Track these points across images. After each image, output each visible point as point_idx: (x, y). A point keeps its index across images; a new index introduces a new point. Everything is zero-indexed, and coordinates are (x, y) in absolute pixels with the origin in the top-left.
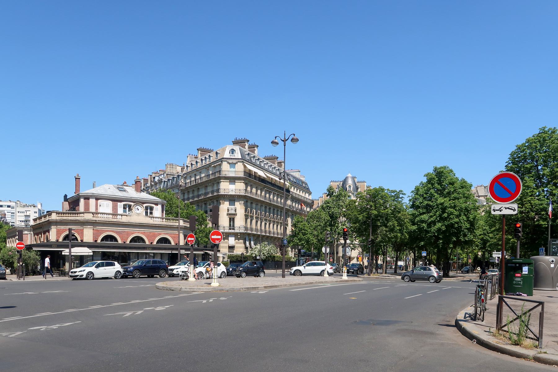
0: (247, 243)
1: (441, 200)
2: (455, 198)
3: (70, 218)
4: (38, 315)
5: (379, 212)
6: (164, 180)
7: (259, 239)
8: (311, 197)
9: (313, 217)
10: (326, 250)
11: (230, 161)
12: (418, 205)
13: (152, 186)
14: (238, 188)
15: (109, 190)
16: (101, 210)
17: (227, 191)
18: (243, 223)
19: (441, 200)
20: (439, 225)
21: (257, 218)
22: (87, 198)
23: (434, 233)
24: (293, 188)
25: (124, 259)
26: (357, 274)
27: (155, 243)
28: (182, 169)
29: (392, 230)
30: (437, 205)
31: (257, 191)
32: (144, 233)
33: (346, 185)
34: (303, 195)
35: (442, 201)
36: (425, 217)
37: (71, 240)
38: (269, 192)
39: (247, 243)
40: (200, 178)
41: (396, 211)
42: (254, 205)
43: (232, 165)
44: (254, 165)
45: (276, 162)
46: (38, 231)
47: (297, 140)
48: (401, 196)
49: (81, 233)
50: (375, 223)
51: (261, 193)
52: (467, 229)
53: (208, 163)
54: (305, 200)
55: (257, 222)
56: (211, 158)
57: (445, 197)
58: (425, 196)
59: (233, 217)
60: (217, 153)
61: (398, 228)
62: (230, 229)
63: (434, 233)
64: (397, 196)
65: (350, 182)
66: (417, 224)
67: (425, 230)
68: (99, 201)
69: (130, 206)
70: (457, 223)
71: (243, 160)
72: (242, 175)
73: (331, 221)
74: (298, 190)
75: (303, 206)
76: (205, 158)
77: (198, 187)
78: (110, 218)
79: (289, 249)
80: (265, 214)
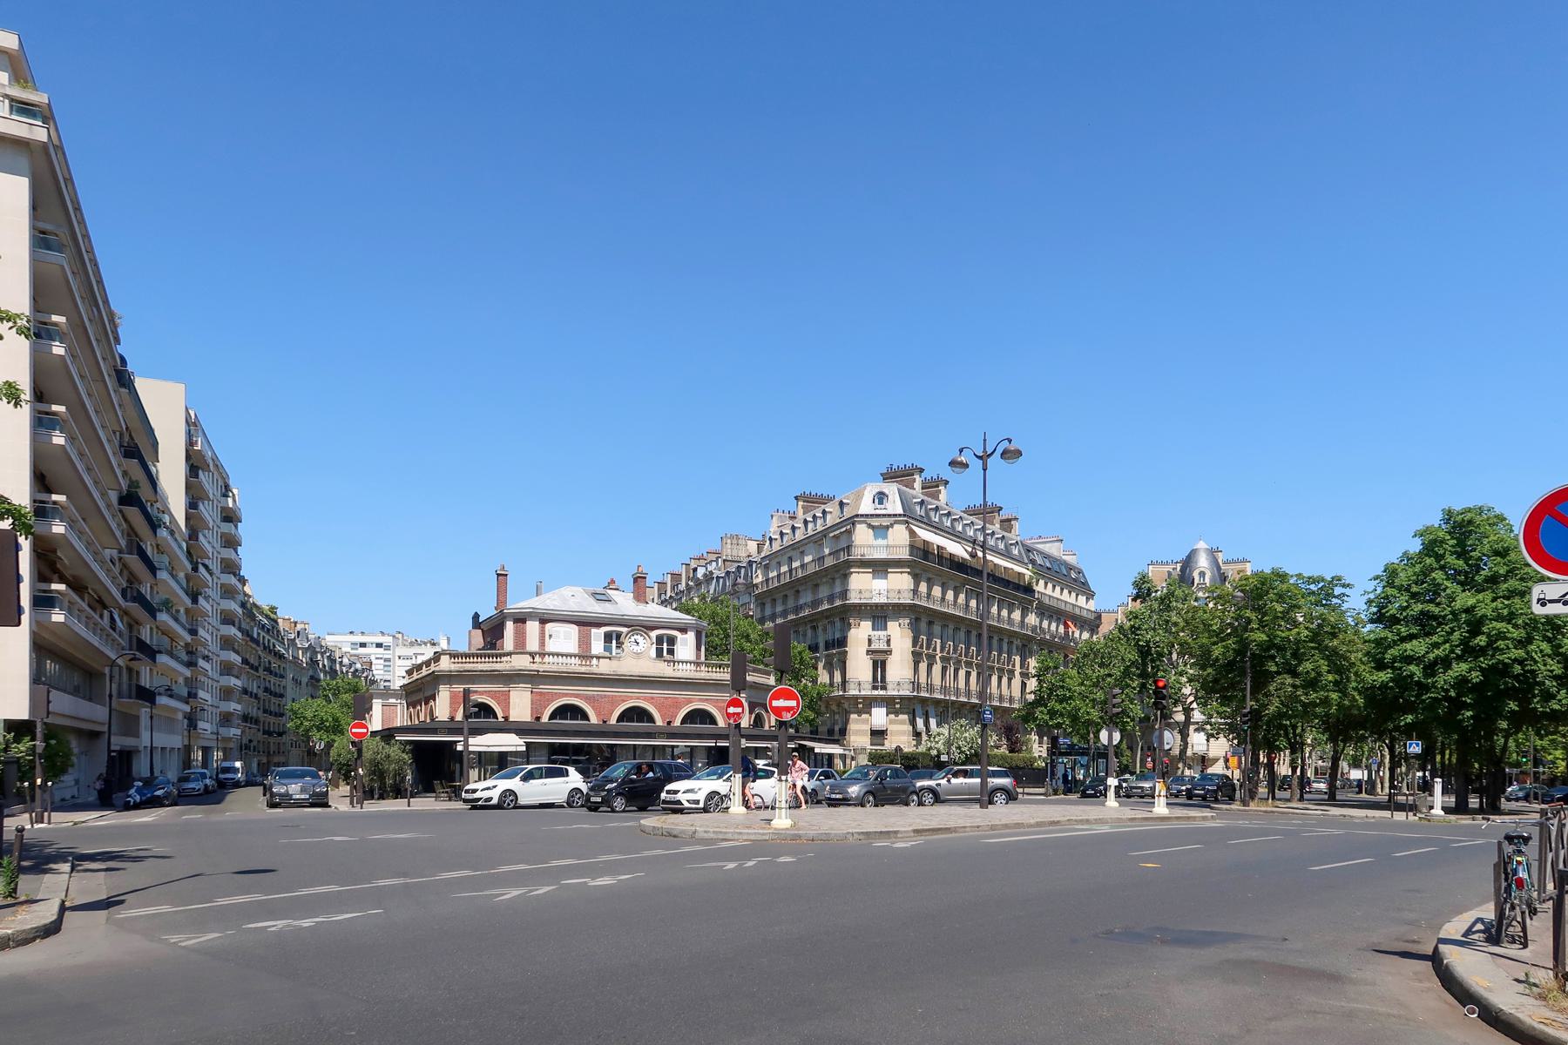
0: (920, 722)
1: (1465, 599)
2: (1511, 594)
3: (480, 667)
4: (305, 892)
5: (1272, 637)
6: (716, 573)
7: (947, 710)
8: (1092, 605)
9: (1091, 652)
10: (1110, 738)
11: (875, 522)
12: (1393, 616)
13: (689, 588)
14: (896, 587)
15: (573, 598)
16: (551, 646)
17: (867, 595)
18: (908, 673)
19: (1465, 599)
20: (1460, 668)
21: (944, 660)
22: (520, 620)
23: (1447, 691)
24: (1042, 582)
25: (589, 759)
26: (1216, 801)
27: (677, 723)
28: (760, 547)
29: (1312, 684)
30: (1452, 613)
31: (944, 594)
32: (651, 700)
33: (1191, 572)
34: (1072, 599)
35: (1471, 602)
36: (1417, 647)
37: (482, 716)
38: (974, 596)
39: (920, 722)
40: (803, 566)
41: (1324, 635)
42: (937, 629)
43: (881, 531)
44: (937, 528)
45: (997, 520)
46: (414, 698)
47: (1018, 453)
48: (1338, 591)
49: (505, 700)
50: (1263, 665)
51: (956, 597)
52: (1556, 678)
53: (820, 528)
54: (1077, 611)
55: (944, 669)
56: (828, 517)
57: (1479, 591)
58: (1415, 589)
59: (880, 657)
60: (841, 504)
61: (1330, 678)
62: (875, 688)
63: (1447, 691)
64: (1326, 591)
65: (1203, 562)
66: (1393, 668)
67: (1419, 683)
68: (549, 626)
69: (619, 636)
70: (1521, 662)
71: (907, 517)
72: (904, 554)
73: (1145, 664)
74: (1050, 586)
75: (1072, 628)
76: (814, 517)
77: (795, 586)
78: (574, 665)
79: (1034, 737)
80: (968, 649)
